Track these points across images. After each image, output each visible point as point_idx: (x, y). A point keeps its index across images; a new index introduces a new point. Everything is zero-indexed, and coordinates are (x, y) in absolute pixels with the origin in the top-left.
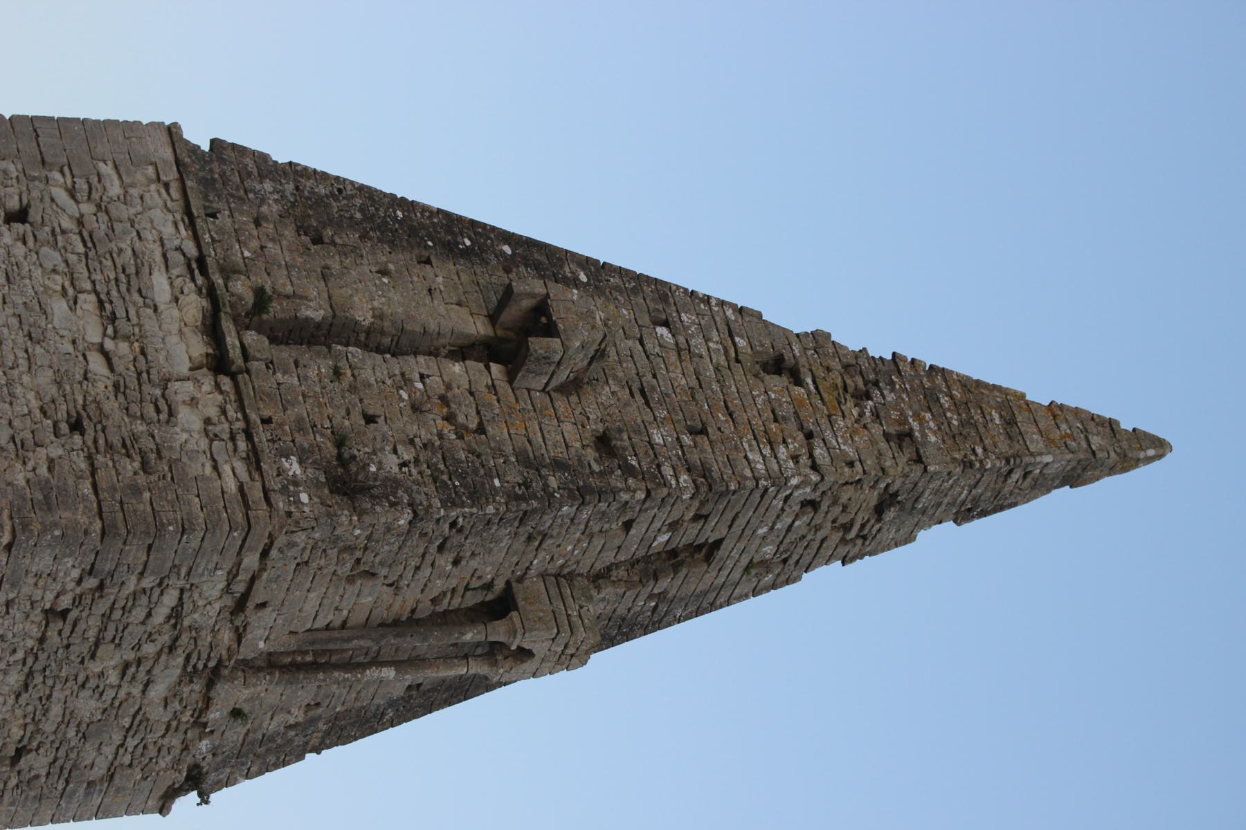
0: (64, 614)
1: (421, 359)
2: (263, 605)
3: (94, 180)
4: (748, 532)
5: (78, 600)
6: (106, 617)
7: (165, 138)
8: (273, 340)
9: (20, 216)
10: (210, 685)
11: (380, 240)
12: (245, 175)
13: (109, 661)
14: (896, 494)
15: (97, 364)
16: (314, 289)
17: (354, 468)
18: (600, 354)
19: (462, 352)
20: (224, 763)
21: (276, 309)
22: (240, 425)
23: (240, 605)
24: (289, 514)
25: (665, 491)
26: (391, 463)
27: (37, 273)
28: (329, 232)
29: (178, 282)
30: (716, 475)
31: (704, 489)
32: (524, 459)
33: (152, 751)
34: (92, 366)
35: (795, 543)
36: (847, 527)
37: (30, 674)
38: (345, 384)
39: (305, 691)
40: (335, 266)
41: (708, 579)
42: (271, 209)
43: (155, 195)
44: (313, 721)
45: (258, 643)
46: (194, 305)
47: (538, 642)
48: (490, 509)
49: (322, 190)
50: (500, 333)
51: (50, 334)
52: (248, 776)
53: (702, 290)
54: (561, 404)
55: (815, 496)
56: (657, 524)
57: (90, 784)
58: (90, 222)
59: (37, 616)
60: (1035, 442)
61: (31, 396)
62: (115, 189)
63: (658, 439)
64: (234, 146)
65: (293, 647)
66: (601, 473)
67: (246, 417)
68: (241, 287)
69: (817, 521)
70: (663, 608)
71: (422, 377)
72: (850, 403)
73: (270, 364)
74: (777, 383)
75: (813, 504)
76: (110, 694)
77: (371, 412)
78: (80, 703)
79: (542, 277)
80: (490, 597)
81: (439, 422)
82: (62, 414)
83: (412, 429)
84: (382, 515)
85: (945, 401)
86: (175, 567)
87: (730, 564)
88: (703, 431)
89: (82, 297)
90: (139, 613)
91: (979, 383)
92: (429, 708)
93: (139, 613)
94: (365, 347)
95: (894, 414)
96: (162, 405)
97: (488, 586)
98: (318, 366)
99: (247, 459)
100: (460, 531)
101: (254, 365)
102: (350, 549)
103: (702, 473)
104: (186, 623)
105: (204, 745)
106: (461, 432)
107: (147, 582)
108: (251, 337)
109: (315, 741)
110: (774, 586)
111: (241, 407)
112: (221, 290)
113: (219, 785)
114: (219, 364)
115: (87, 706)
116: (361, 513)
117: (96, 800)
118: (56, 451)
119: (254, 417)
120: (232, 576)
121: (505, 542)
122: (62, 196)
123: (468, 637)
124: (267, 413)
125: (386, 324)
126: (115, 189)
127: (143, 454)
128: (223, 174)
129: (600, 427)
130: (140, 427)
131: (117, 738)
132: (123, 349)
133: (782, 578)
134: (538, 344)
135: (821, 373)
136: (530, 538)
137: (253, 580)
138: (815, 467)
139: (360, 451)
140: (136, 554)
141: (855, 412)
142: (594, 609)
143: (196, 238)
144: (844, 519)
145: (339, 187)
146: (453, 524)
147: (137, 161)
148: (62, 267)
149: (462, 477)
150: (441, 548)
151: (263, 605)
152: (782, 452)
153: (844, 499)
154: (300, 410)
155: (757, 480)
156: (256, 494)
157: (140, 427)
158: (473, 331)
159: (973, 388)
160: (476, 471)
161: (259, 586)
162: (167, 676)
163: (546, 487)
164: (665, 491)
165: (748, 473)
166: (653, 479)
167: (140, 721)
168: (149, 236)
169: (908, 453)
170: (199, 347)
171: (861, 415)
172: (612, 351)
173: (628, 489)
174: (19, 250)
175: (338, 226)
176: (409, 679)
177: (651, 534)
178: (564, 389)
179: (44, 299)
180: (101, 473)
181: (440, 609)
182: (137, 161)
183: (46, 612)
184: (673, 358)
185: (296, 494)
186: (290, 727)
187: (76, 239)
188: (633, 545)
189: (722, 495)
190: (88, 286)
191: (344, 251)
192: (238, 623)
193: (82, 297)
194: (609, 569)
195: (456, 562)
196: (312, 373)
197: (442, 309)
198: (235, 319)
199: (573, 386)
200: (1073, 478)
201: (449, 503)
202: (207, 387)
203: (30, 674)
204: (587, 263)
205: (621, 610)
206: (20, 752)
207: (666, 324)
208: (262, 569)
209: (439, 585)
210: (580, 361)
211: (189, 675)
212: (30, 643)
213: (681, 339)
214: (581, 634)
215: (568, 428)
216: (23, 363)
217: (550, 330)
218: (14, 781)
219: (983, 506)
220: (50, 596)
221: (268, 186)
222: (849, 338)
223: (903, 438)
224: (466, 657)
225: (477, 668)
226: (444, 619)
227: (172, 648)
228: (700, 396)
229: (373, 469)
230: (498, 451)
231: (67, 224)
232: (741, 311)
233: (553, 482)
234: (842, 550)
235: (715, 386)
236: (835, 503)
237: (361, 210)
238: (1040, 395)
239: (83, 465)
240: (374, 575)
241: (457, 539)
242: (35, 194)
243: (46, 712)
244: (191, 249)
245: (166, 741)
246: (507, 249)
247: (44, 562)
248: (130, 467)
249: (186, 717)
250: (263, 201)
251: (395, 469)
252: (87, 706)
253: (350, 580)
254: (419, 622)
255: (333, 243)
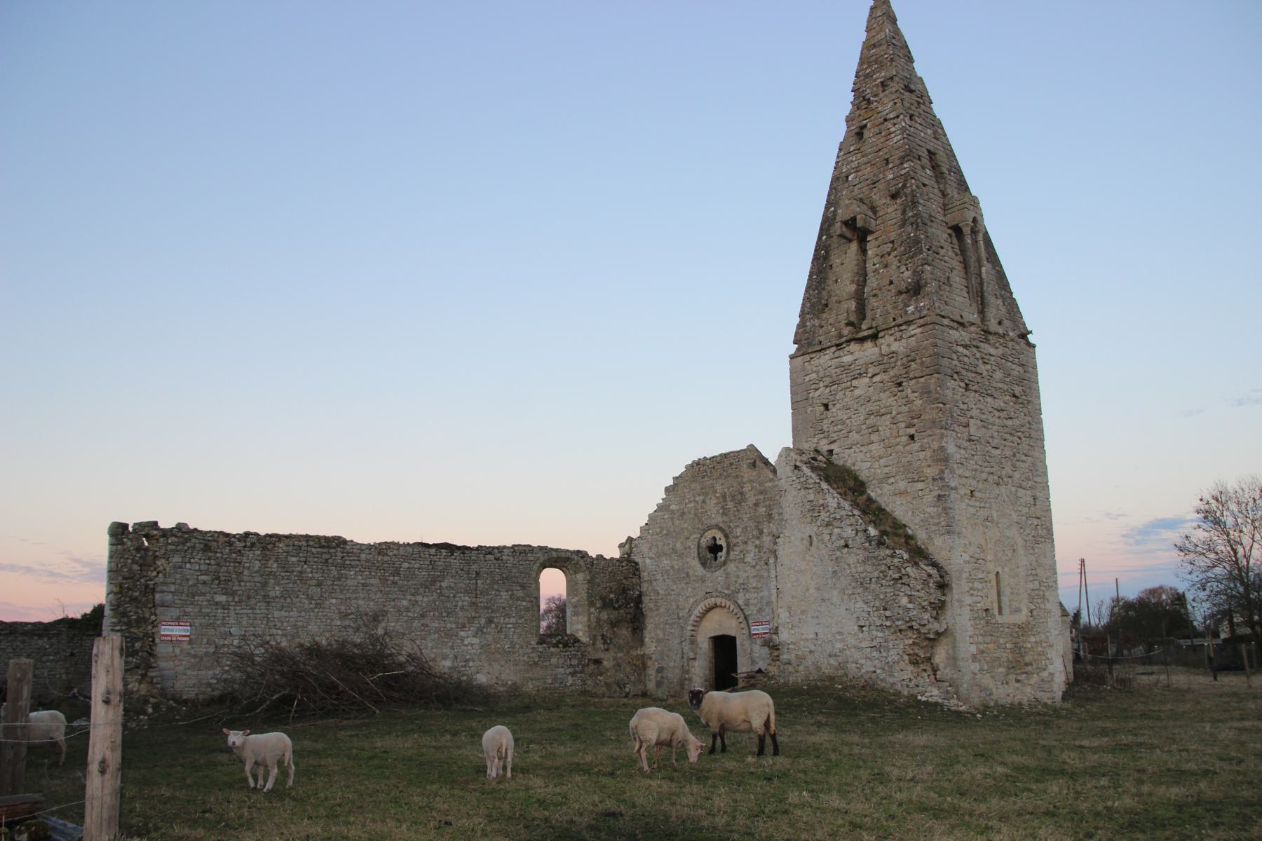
0: (967, 385)
1: (867, 266)
2: (961, 316)
3: (811, 383)
4: (924, 140)
5: (962, 380)
6: (967, 370)
7: (794, 360)
8: (864, 318)
9: (826, 406)
10: (990, 333)
11: (825, 283)
12: (805, 332)
13: (982, 368)
14: (905, 86)
15: (877, 379)
16: (845, 306)
17: (910, 287)
18: (861, 200)
19: (864, 251)
20: (1018, 326)
21: (853, 318)
22: (896, 328)
23: (962, 324)
24: (928, 309)
25: (911, 172)
26: (907, 274)
27: (845, 399)
28: (823, 301)
29: (846, 353)
30: (903, 154)
31: (909, 158)
32: (903, 225)
33: (1014, 352)
34: (878, 380)
35: (926, 122)
36: (919, 103)
37: (987, 395)
38: (879, 292)
39: (991, 299)
40: (835, 299)
41: (941, 154)
42: (816, 322)
43: (814, 362)
44: (1002, 296)
45: (974, 317)
46: (854, 347)
47: (970, 215)
48: (922, 236)
49: (808, 305)
50: (855, 238)
51: (867, 395)
52: (1022, 317)
53: (834, 165)
54: (880, 213)
55: (908, 115)
56: (923, 174)
57: (1025, 372)
58: (826, 383)
59: (967, 393)
60: (881, 36)
61: (889, 400)
62: (814, 375)
63: (891, 176)
64: (795, 336)
65: (975, 305)
66: (906, 196)
67: (894, 327)
68: (846, 331)
69: (917, 114)
70: (954, 170)
71: (874, 265)
72: (872, 106)
73: (873, 319)
74: (866, 133)
75: (911, 117)
76: (994, 367)
77: (888, 282)
78: (997, 377)
79: (833, 224)
80: (954, 234)
81: (891, 257)
82: (896, 389)
83: (894, 267)
84: (927, 276)
85: (868, 71)
86: (949, 348)
87: (936, 146)
88: (887, 160)
89: (853, 385)
90: (966, 359)
91: (860, 59)
92: (995, 254)
93: (966, 359)
94: (864, 286)
95: (875, 89)
96: (890, 356)
97: (950, 235)
98: (873, 302)
99: (909, 325)
100: (931, 247)
101: (874, 325)
102: (940, 286)
103: (903, 159)
104: (968, 343)
105: (1011, 334)
106: (894, 249)
107: (955, 357)
108: (864, 327)
109: (1009, 295)
110: (942, 128)
111: (890, 328)
112: (848, 338)
113: (1025, 328)
114: (874, 337)
115: (999, 375)
116: (926, 283)
117: (1031, 369)
118: (909, 391)
119: (893, 324)
120: (952, 328)
121: (934, 230)
122: (818, 393)
123: (969, 241)
124: (891, 319)
125: (856, 279)
126: (814, 375)
127: (908, 362)
128: (805, 340)
129: (889, 198)
130: (899, 363)
131: (1009, 364)
132: (871, 371)
133: (939, 126)
134: (859, 224)
135: (861, 118)
136: (932, 221)
137: (953, 321)
138: (898, 117)
139: (903, 286)
140: (945, 362)
141: (875, 104)
142: (956, 196)
143: (829, 347)
144: (916, 104)
145: (807, 299)
146: (929, 250)
147: (804, 369)
148: (843, 392)
149: (910, 248)
150: (938, 254)
151: (961, 316)
152: (893, 129)
153: (909, 105)
154: (889, 308)
155: (904, 138)
156: (921, 321)
157: (899, 363)
158: (856, 248)
159: (863, 61)
160: (908, 243)
161: (954, 318)
162: (987, 348)
163: (913, 217)
164: (911, 172)
165: (901, 142)
166: (907, 177)
167: (1003, 357)
168: (830, 364)
169: (889, 82)
170: (869, 344)
171: (876, 101)
172: (859, 196)
173: (911, 186)
174: (838, 406)
175: (820, 299)
176: (985, 262)
177: (927, 176)
178: (875, 212)
179: (855, 397)
180: (917, 375)
181: (959, 252)
182: (804, 369)
183: (966, 390)
184: (860, 173)
185: (921, 307)
186: (1004, 304)
187: (833, 388)
188: (932, 183)
189: (911, 151)
190: (849, 383)
191: (830, 296)
192: (967, 325)
193: (853, 385)
194: (941, 191)
195: (942, 248)
196: (875, 304)
197: (848, 260)
198: (857, 332)
199: (874, 209)
200: (893, 20)
201: (921, 252)
202: (883, 341)
203: (987, 395)
204: (827, 208)
205: (955, 185)
206: (1014, 396)
207: (847, 177)
208: (948, 317)
209: (951, 253)
210: (864, 207)
211: (987, 341)
212: (977, 395)
213: (852, 171)
214: (966, 199)
215: (889, 210)
216: (878, 403)
217: (854, 219)
218: (1024, 397)
219: (907, 53)
220: (961, 390)
221: (808, 324)
222: (847, 108)
223: (883, 85)
224: (976, 242)
225: (980, 237)
226: (963, 251)
227: (978, 347)
228: (873, 162)
229: (910, 280)
230: (900, 235)
231: (828, 390)
232: (840, 150)
233: (910, 214)
234: (927, 104)
235: (870, 157)
236: (910, 108)
237: (814, 291)
238: (863, 36)
239: (914, 381)
240: (948, 278)
241: (934, 248)
242: (818, 401)
243: (1000, 388)
244: (834, 349)
245: (1010, 347)
246: (824, 237)
247: (949, 392)
248: (913, 365)
249: (1002, 341)
250: (814, 325)
251: (909, 272)
252: (999, 375)
253: (950, 286)
254: (965, 260)
255: (827, 300)
